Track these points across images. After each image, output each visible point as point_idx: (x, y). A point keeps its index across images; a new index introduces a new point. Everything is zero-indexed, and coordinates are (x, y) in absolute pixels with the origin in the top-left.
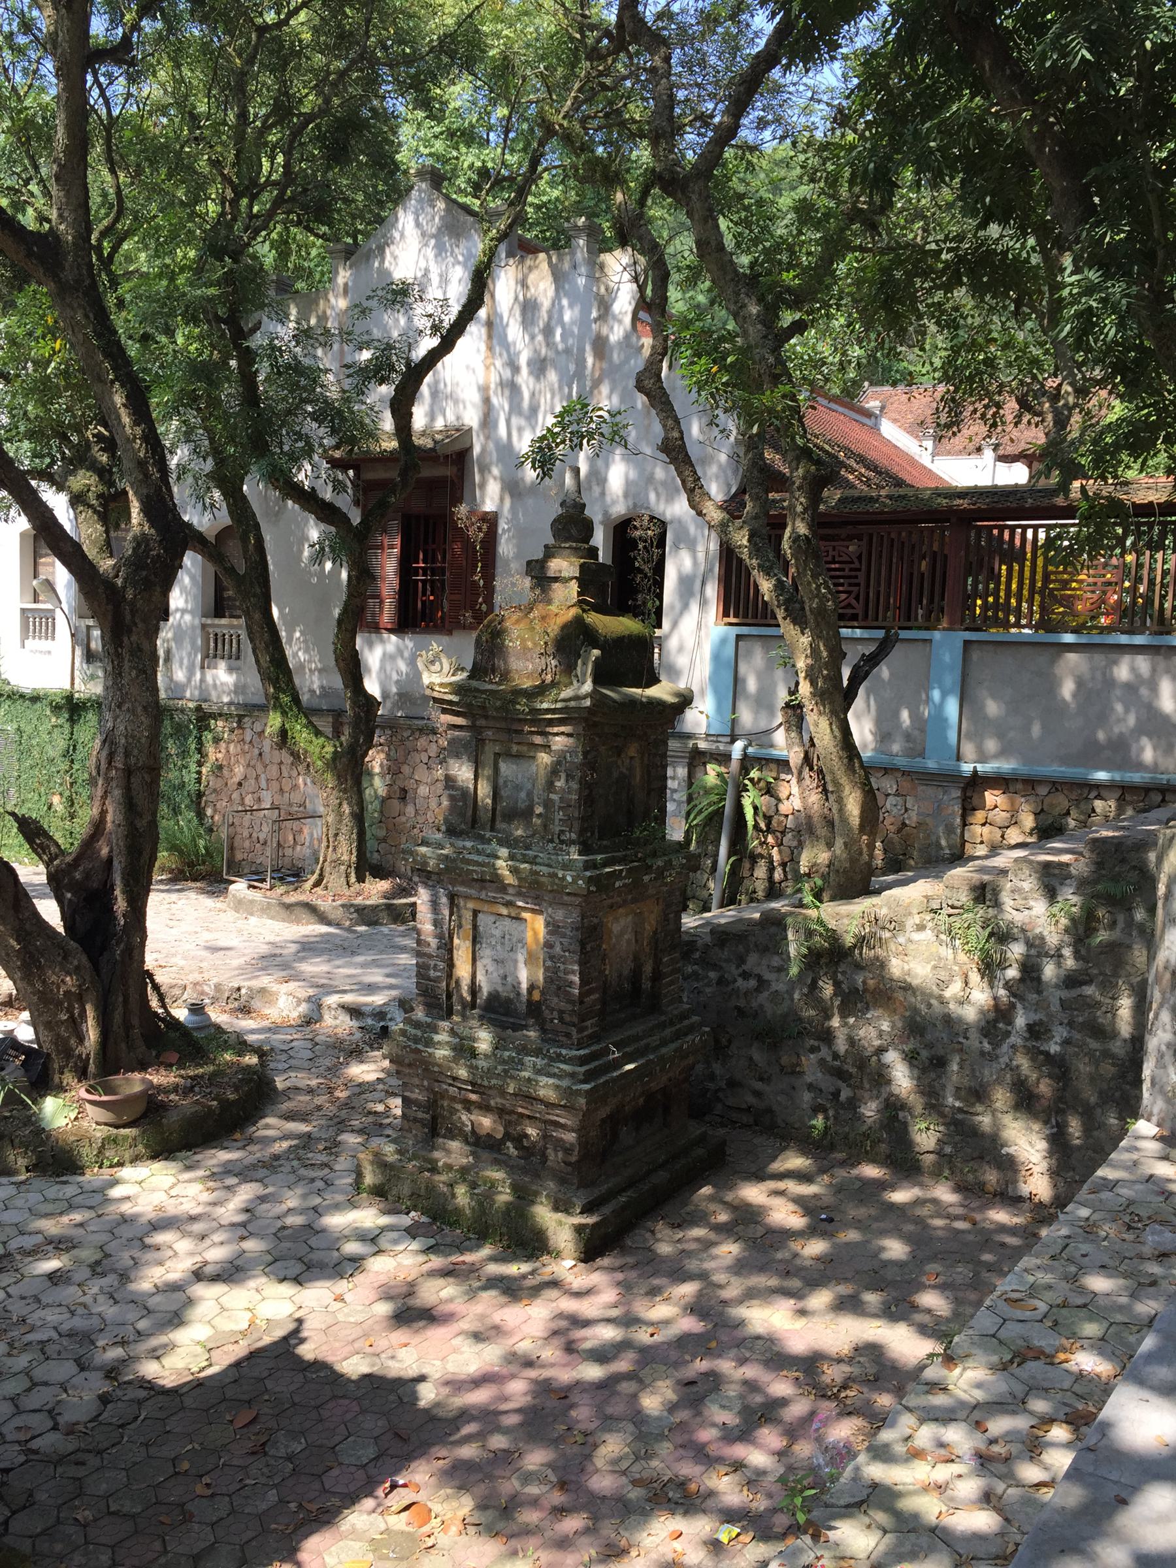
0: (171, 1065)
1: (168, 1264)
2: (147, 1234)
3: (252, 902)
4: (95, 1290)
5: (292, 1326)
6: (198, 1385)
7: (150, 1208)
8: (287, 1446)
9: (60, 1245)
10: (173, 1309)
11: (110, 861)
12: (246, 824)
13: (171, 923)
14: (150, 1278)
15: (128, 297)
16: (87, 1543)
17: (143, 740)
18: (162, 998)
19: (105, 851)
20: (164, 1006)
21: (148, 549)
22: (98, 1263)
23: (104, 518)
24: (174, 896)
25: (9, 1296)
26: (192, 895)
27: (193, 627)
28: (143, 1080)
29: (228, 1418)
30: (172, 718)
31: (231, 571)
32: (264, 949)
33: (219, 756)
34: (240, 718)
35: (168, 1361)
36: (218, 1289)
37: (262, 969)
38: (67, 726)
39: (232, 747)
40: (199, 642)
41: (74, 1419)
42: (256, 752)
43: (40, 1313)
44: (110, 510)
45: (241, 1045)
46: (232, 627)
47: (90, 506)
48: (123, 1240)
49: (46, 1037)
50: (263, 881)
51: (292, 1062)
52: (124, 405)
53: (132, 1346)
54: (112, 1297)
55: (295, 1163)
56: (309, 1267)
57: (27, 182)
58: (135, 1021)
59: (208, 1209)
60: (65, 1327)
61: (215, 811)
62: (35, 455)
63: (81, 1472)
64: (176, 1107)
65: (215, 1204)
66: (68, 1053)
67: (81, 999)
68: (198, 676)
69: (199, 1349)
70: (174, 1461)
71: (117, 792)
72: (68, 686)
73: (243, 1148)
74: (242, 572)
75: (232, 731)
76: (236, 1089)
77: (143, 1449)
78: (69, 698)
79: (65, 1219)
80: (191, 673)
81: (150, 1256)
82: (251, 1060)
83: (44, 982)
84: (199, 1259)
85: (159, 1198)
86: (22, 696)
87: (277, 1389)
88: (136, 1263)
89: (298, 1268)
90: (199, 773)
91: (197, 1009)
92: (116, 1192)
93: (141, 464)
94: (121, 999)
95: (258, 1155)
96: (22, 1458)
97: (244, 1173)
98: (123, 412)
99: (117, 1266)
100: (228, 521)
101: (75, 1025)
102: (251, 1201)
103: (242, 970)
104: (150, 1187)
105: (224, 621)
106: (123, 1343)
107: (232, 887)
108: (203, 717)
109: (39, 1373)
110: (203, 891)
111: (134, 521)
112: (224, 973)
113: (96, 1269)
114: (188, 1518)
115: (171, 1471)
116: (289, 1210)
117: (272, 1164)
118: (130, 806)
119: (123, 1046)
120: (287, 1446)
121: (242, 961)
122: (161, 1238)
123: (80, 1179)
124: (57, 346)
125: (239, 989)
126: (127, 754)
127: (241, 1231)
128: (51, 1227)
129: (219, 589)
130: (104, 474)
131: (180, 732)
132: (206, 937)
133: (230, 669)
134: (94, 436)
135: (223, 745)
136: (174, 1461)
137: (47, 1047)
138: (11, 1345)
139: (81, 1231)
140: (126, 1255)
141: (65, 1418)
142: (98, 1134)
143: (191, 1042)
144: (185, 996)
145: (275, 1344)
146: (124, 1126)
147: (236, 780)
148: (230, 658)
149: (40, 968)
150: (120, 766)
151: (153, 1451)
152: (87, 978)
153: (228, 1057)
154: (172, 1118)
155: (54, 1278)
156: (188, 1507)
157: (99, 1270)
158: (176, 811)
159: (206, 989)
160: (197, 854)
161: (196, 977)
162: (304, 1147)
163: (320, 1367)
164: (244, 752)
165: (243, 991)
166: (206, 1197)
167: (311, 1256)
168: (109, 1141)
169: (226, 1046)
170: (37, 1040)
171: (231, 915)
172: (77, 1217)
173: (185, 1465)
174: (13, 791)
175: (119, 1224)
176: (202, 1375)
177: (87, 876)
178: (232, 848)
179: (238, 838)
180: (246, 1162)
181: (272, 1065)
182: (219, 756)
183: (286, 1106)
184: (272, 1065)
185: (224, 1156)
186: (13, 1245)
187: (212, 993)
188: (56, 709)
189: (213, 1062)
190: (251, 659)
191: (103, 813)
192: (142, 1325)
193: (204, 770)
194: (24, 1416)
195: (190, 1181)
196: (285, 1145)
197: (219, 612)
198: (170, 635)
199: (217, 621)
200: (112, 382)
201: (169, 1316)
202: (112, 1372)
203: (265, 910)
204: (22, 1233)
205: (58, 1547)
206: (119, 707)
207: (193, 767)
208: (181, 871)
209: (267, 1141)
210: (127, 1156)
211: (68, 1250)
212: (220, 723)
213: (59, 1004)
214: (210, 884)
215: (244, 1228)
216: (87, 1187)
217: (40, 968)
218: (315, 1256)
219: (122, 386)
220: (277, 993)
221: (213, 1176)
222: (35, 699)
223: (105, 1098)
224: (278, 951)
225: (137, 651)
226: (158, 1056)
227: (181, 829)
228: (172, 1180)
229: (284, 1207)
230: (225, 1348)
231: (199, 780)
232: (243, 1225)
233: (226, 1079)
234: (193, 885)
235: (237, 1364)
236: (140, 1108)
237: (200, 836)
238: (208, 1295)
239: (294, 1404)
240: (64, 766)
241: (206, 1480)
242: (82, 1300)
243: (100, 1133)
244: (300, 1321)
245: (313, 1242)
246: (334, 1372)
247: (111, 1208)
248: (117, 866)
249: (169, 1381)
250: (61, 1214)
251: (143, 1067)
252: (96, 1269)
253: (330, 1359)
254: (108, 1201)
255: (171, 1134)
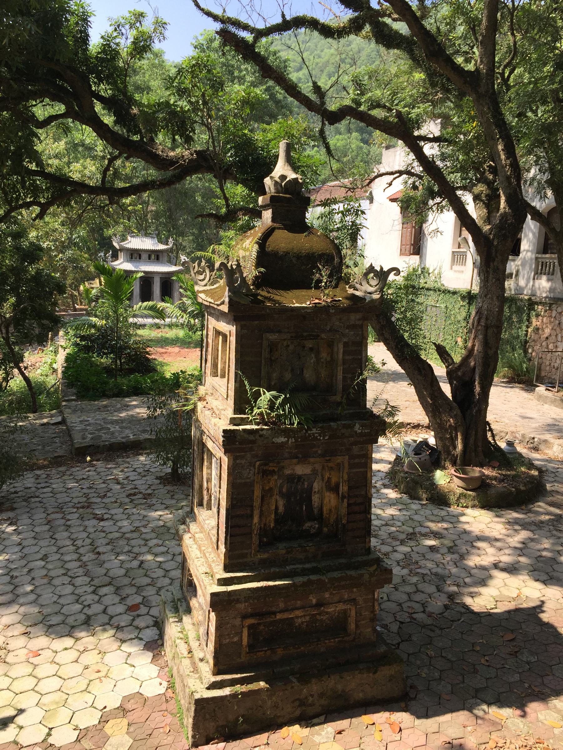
0: (495, 468)
1: (482, 557)
2: (475, 541)
3: (546, 397)
4: (448, 559)
5: (539, 603)
6: (489, 615)
7: (478, 530)
8: (527, 657)
9: (436, 535)
10: (482, 578)
11: (474, 368)
12: (548, 358)
13: (505, 402)
14: (473, 561)
15: (513, 96)
16: (430, 665)
17: (495, 313)
18: (493, 436)
19: (472, 364)
20: (494, 439)
21: (506, 220)
22: (451, 547)
23: (487, 206)
24: (508, 390)
25: (413, 551)
26: (517, 390)
27: (531, 259)
28: (480, 471)
29: (501, 634)
30: (516, 304)
31: (553, 230)
32: (550, 421)
33: (538, 323)
34: (551, 305)
35: (477, 600)
36: (504, 575)
37: (547, 431)
38: (467, 306)
39: (545, 319)
40: (534, 266)
41: (432, 611)
42: (557, 322)
43: (424, 562)
44: (490, 202)
45: (530, 465)
46: (551, 258)
47: (482, 201)
48: (464, 541)
49: (440, 444)
50: (554, 387)
51: (557, 479)
52: (503, 150)
53: (461, 588)
54: (455, 564)
55: (551, 527)
56: (551, 578)
57: (472, 47)
58: (480, 444)
59: (505, 537)
60: (434, 571)
61: (533, 351)
62: (462, 179)
63: (432, 634)
64: (495, 487)
65: (508, 536)
66: (449, 453)
67: (456, 429)
68: (531, 283)
69: (492, 599)
70: (473, 645)
71: (481, 337)
72: (469, 288)
73: (526, 514)
74: (558, 230)
75: (546, 311)
76: (525, 485)
77: (460, 634)
78: (469, 293)
79: (440, 525)
80: (528, 282)
81: (475, 551)
82: (535, 473)
83: (441, 419)
84: (497, 559)
85: (482, 527)
86: (449, 292)
87: (527, 630)
88: (468, 553)
89: (545, 577)
90: (527, 331)
91: (510, 444)
92: (463, 519)
93: (508, 178)
94: (474, 432)
95: (532, 519)
96: (409, 620)
97: (525, 526)
98: (502, 153)
99: (459, 551)
100: (554, 204)
101: (453, 440)
102: (525, 539)
103: (536, 429)
104: (478, 520)
105: (547, 256)
106: (458, 586)
107: (537, 389)
108: (531, 304)
109: (420, 586)
110: (523, 389)
111: (502, 206)
112: (527, 429)
113: (451, 550)
114: (476, 671)
115: (471, 648)
116: (545, 549)
117: (539, 525)
118: (486, 344)
119: (473, 454)
120: (525, 657)
121: (537, 425)
122: (480, 544)
123: (449, 509)
124: (474, 125)
125: (534, 438)
126: (487, 319)
127: (518, 552)
128: (433, 526)
129: (546, 239)
130: (489, 184)
131: (519, 311)
132: (521, 411)
133: (548, 280)
134: (487, 166)
135: (540, 318)
136: (473, 645)
137: (440, 448)
138: (411, 571)
139: (446, 532)
140: (464, 548)
141: (429, 609)
142: (458, 491)
143: (506, 459)
144: (507, 437)
145: (529, 608)
146: (470, 490)
147: (545, 336)
148: (549, 274)
149: (440, 413)
150: (483, 324)
151: (464, 637)
152: (460, 420)
153: (523, 469)
154: (492, 492)
155: (431, 548)
156: (476, 666)
157: (451, 551)
158: (514, 349)
159: (517, 435)
160: (522, 371)
161: (513, 429)
162: (557, 521)
163: (549, 626)
164: (551, 322)
165: (536, 440)
166: (504, 531)
167: (552, 573)
168: (461, 495)
169: (523, 464)
170: (436, 445)
171: (535, 402)
172: (445, 525)
173: (478, 648)
174: (441, 334)
175: (463, 533)
176: (492, 611)
177: (464, 374)
178: (540, 369)
179: (543, 365)
180: (526, 520)
181: (546, 478)
182: (538, 323)
183: (550, 499)
184: (546, 478)
185: (515, 515)
186: (418, 530)
187: (520, 438)
188: (463, 298)
189: (515, 470)
190: (559, 274)
191: (473, 346)
192: (467, 580)
193: (530, 330)
194: (412, 603)
195: (498, 522)
196: (547, 517)
197: (545, 251)
198: (519, 263)
199: (544, 256)
200: (498, 139)
201: (480, 580)
202: (451, 597)
203: (553, 402)
204: (421, 526)
205: (418, 662)
206: (486, 296)
207: (524, 328)
208: (513, 378)
209: (538, 513)
210: (470, 504)
211: (439, 538)
212: (540, 307)
213: (446, 430)
214: (527, 386)
215: (523, 549)
216: (451, 513)
217: (440, 413)
218: (555, 574)
219: (503, 141)
220: (553, 444)
221: (509, 523)
222: (454, 293)
223: (462, 476)
224: (557, 423)
225: (496, 270)
226: (489, 462)
227: (515, 358)
228: (489, 520)
229: (542, 547)
230: (504, 603)
231: (526, 335)
232: (521, 549)
233: (520, 480)
234: (518, 385)
235: (509, 612)
236: (478, 484)
237: (524, 362)
238: (500, 577)
239: (534, 639)
240: (464, 324)
241: (487, 658)
242: (443, 561)
243: (459, 491)
244: (543, 602)
245: (555, 567)
246: (557, 631)
247: (460, 525)
248: (477, 372)
249: (476, 609)
250: (438, 522)
251: (482, 466)
252: (451, 550)
253: (556, 624)
254: (459, 522)
255: (491, 499)
